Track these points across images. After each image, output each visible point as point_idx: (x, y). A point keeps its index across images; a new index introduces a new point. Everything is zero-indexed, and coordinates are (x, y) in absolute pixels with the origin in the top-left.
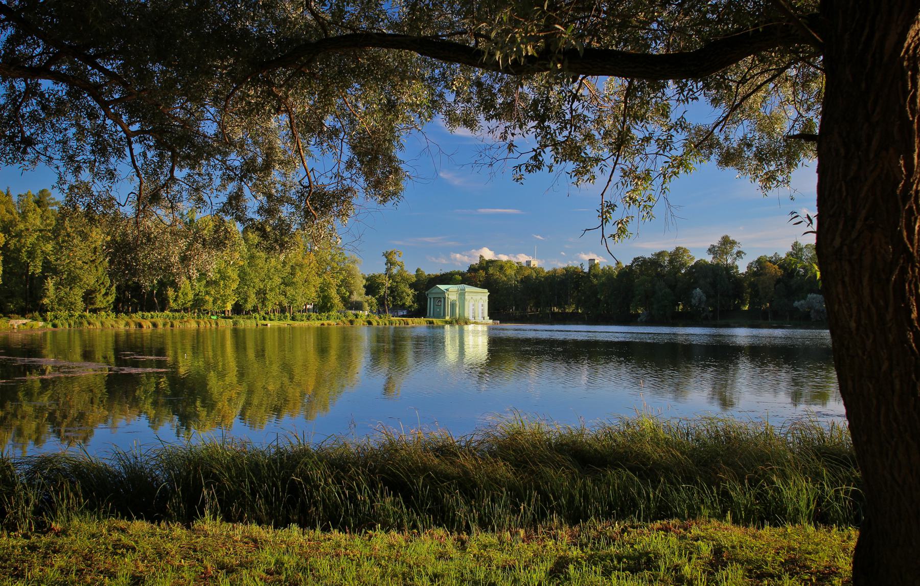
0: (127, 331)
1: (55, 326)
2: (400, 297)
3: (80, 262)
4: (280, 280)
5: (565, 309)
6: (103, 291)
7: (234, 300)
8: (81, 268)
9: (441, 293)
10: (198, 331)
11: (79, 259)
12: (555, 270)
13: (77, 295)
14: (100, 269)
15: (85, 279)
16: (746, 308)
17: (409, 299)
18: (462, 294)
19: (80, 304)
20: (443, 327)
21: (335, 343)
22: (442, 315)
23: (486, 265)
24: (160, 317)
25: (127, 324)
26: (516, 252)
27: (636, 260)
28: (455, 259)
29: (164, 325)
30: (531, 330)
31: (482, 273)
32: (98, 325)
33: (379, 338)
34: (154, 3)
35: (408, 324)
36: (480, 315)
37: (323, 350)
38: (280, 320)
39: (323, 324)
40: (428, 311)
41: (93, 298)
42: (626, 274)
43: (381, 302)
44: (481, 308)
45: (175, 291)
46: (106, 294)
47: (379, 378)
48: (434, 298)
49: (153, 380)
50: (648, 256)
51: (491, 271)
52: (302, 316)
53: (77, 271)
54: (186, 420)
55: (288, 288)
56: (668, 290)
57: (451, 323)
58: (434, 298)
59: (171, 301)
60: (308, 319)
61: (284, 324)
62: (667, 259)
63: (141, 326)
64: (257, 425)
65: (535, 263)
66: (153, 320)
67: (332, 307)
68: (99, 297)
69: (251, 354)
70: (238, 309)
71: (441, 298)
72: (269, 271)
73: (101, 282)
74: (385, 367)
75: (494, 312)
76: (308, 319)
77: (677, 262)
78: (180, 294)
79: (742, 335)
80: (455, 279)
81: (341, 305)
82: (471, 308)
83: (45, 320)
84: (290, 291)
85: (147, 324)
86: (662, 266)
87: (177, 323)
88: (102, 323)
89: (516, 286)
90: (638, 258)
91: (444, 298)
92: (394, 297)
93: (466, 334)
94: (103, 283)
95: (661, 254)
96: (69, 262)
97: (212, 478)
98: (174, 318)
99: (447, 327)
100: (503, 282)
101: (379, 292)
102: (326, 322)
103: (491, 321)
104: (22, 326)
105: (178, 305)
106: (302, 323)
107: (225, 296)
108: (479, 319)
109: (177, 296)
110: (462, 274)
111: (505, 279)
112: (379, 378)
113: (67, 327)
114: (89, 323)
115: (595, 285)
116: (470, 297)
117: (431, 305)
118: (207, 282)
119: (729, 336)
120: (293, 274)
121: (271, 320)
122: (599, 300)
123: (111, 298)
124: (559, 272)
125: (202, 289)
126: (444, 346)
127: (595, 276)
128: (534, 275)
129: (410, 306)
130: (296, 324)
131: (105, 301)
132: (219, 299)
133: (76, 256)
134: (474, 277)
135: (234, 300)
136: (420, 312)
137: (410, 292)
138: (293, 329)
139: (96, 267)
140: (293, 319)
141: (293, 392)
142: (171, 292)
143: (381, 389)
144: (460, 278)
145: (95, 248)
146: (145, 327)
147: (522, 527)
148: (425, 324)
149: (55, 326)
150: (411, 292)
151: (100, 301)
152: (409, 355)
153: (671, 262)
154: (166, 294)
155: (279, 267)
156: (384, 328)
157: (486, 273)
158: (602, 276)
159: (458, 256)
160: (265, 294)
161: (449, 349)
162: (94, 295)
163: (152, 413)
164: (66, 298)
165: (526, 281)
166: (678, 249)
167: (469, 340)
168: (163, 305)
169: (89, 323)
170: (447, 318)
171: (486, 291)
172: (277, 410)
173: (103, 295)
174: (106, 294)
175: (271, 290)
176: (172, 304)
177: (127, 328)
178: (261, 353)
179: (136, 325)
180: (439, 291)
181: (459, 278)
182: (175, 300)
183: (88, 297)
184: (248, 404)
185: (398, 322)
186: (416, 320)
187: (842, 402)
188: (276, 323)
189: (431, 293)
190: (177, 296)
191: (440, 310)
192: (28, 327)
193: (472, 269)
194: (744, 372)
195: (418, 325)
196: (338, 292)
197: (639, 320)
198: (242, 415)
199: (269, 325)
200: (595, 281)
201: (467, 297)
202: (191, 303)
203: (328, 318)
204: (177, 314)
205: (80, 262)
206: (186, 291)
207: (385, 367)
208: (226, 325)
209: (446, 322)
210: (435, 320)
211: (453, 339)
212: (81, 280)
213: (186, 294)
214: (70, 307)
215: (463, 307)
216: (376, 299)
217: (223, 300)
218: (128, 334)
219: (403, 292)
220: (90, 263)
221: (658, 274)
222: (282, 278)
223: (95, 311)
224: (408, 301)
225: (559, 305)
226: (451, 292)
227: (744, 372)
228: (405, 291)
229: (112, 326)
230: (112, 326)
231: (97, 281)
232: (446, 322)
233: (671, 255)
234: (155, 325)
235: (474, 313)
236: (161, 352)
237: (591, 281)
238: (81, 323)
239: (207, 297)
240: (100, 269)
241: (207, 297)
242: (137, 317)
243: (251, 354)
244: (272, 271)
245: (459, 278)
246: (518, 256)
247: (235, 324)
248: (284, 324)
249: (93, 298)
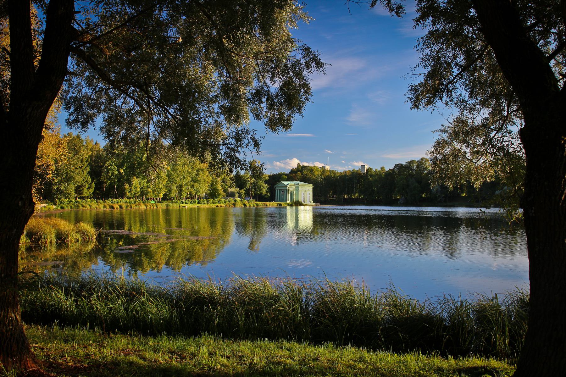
0: (104, 211)
1: (62, 208)
2: (259, 189)
3: (74, 168)
4: (191, 179)
5: (351, 196)
6: (87, 186)
7: (165, 191)
8: (74, 172)
9: (284, 187)
10: (146, 210)
11: (73, 166)
12: (345, 172)
13: (71, 189)
14: (85, 172)
15: (77, 179)
16: (464, 195)
17: (264, 189)
18: (297, 186)
19: (73, 194)
20: (286, 207)
21: (220, 218)
22: (285, 200)
23: (301, 169)
24: (123, 202)
25: (105, 206)
26: (313, 161)
27: (396, 165)
28: (276, 166)
29: (127, 207)
30: (339, 209)
31: (299, 174)
32: (89, 208)
33: (247, 213)
34: (182, 1)
35: (267, 206)
36: (308, 200)
37: (213, 223)
38: (191, 203)
39: (217, 206)
40: (276, 198)
41: (81, 190)
42: (391, 174)
43: (248, 193)
44: (308, 195)
45: (130, 186)
46: (89, 188)
47: (246, 239)
48: (280, 190)
49: (115, 241)
50: (404, 163)
51: (305, 172)
52: (204, 201)
53: (72, 173)
54: (135, 265)
55: (195, 184)
56: (417, 184)
57: (291, 205)
58: (280, 190)
59: (128, 192)
60: (208, 203)
61: (195, 206)
62: (415, 165)
63: (113, 208)
64: (166, 266)
65: (328, 168)
66: (120, 204)
67: (218, 195)
68: (85, 190)
69: (174, 223)
70: (165, 198)
71: (284, 190)
72: (184, 173)
73: (86, 180)
74: (250, 230)
75: (316, 199)
76: (208, 202)
77: (422, 167)
78: (133, 188)
79: (462, 211)
80: (283, 177)
81: (224, 194)
82: (303, 195)
83: (55, 204)
84: (196, 185)
85: (116, 206)
86: (412, 169)
87: (133, 206)
88: (90, 206)
89: (321, 182)
90: (398, 165)
91: (286, 190)
92: (255, 189)
93: (299, 213)
94: (87, 181)
95: (412, 162)
96: (67, 168)
97: (91, 291)
98: (130, 203)
99: (288, 207)
100: (313, 179)
101: (246, 186)
102: (219, 205)
103: (315, 203)
104: (43, 208)
105: (132, 195)
106: (204, 205)
107: (159, 188)
108: (308, 202)
109: (131, 189)
110: (287, 175)
111: (314, 177)
112: (246, 239)
113: (70, 208)
114: (83, 206)
115: (371, 181)
116: (302, 189)
117: (277, 193)
118: (148, 180)
119: (451, 212)
120: (198, 175)
121: (186, 203)
122: (373, 190)
123: (92, 191)
124: (348, 174)
125: (145, 184)
126: (286, 219)
127: (371, 176)
128: (333, 175)
129: (266, 195)
130: (202, 206)
131: (88, 192)
132: (155, 191)
133: (71, 164)
134: (295, 176)
135: (165, 191)
136: (272, 199)
137: (265, 186)
138: (199, 209)
139: (82, 171)
140: (199, 203)
141: (199, 249)
142: (127, 187)
143: (248, 245)
144: (286, 177)
145: (83, 159)
146: (115, 208)
147: (49, 285)
148: (276, 206)
149: (62, 208)
150: (266, 186)
151: (86, 192)
152: (265, 226)
153: (418, 167)
154: (124, 188)
155: (190, 170)
156: (250, 208)
157: (302, 174)
158: (375, 176)
159: (278, 163)
160: (181, 187)
161: (289, 220)
162: (81, 189)
163: (114, 262)
164: (66, 191)
165: (327, 179)
166: (422, 159)
167: (301, 216)
168: (122, 195)
169: (83, 206)
170: (288, 202)
171: (311, 185)
172: (189, 260)
173: (87, 189)
174: (89, 188)
175: (185, 185)
176: (128, 194)
177: (105, 209)
178: (180, 224)
179: (110, 207)
180: (283, 185)
181: (285, 177)
182: (130, 192)
183: (79, 190)
184: (172, 255)
185: (261, 204)
186: (271, 203)
187: (527, 254)
188: (206, 206)
189: (278, 187)
190: (131, 189)
191: (284, 196)
192: (47, 209)
193: (293, 171)
194: (463, 235)
195: (272, 206)
196: (222, 186)
197: (399, 202)
198: (167, 264)
199: (186, 207)
200: (371, 179)
201: (300, 188)
202: (139, 193)
203: (219, 202)
204: (132, 200)
205: (74, 168)
206: (136, 186)
207: (250, 230)
208: (162, 206)
209: (288, 204)
210: (282, 203)
211: (292, 214)
212: (75, 179)
213: (136, 188)
214: (67, 196)
215: (298, 194)
216: (245, 190)
217: (158, 191)
218: (104, 213)
219: (261, 186)
220: (79, 169)
221: (410, 175)
222: (191, 178)
223: (83, 198)
224: (264, 192)
225: (348, 194)
226: (290, 185)
227: (463, 235)
228: (262, 185)
229: (96, 208)
230: (96, 208)
231: (83, 180)
232: (288, 204)
233: (417, 162)
234: (121, 207)
235: (304, 199)
236: (121, 225)
237: (368, 179)
238: (78, 206)
239: (149, 190)
240: (85, 172)
241: (149, 190)
242: (109, 202)
243: (174, 223)
244: (186, 173)
245: (285, 177)
246: (314, 163)
247: (167, 206)
248: (195, 206)
249: (81, 190)
